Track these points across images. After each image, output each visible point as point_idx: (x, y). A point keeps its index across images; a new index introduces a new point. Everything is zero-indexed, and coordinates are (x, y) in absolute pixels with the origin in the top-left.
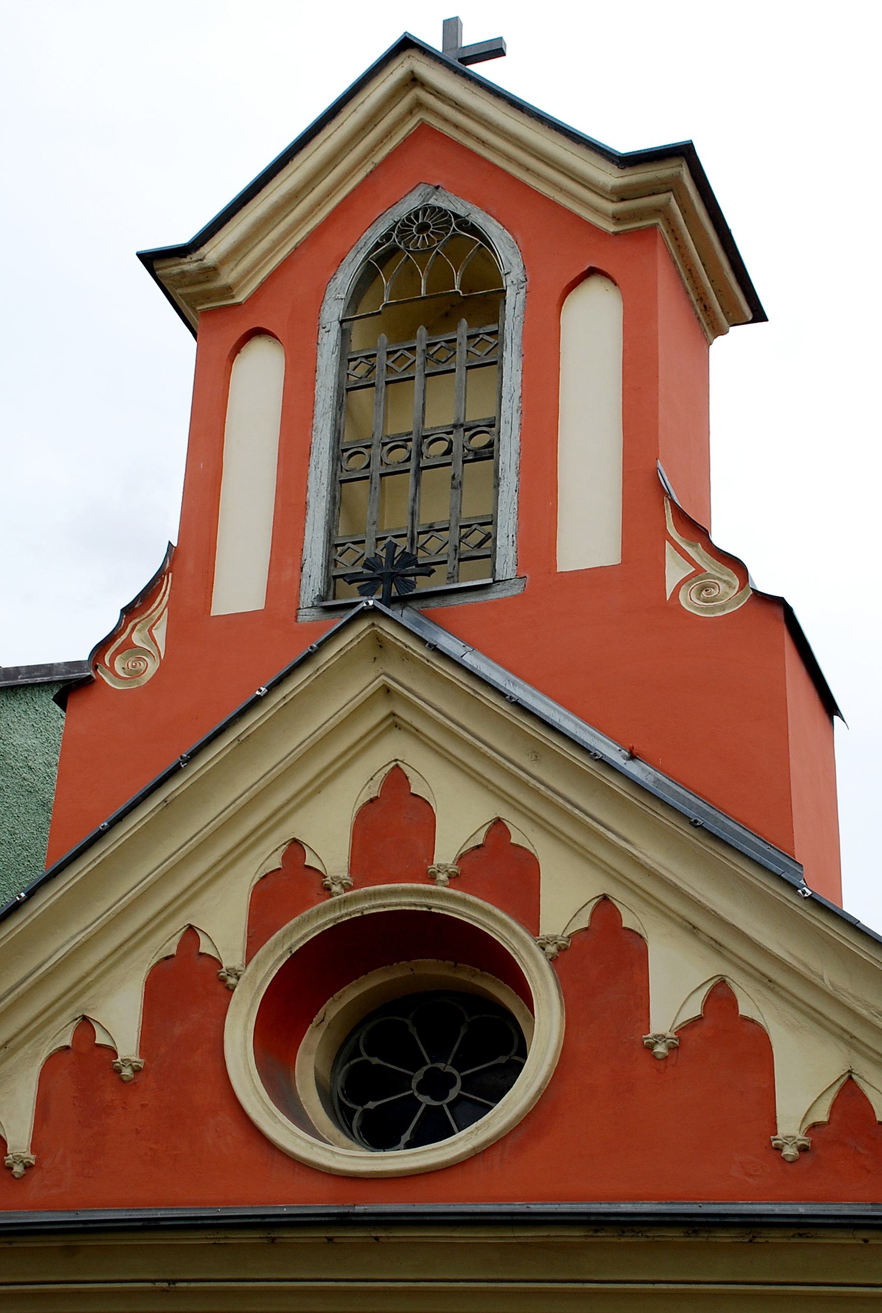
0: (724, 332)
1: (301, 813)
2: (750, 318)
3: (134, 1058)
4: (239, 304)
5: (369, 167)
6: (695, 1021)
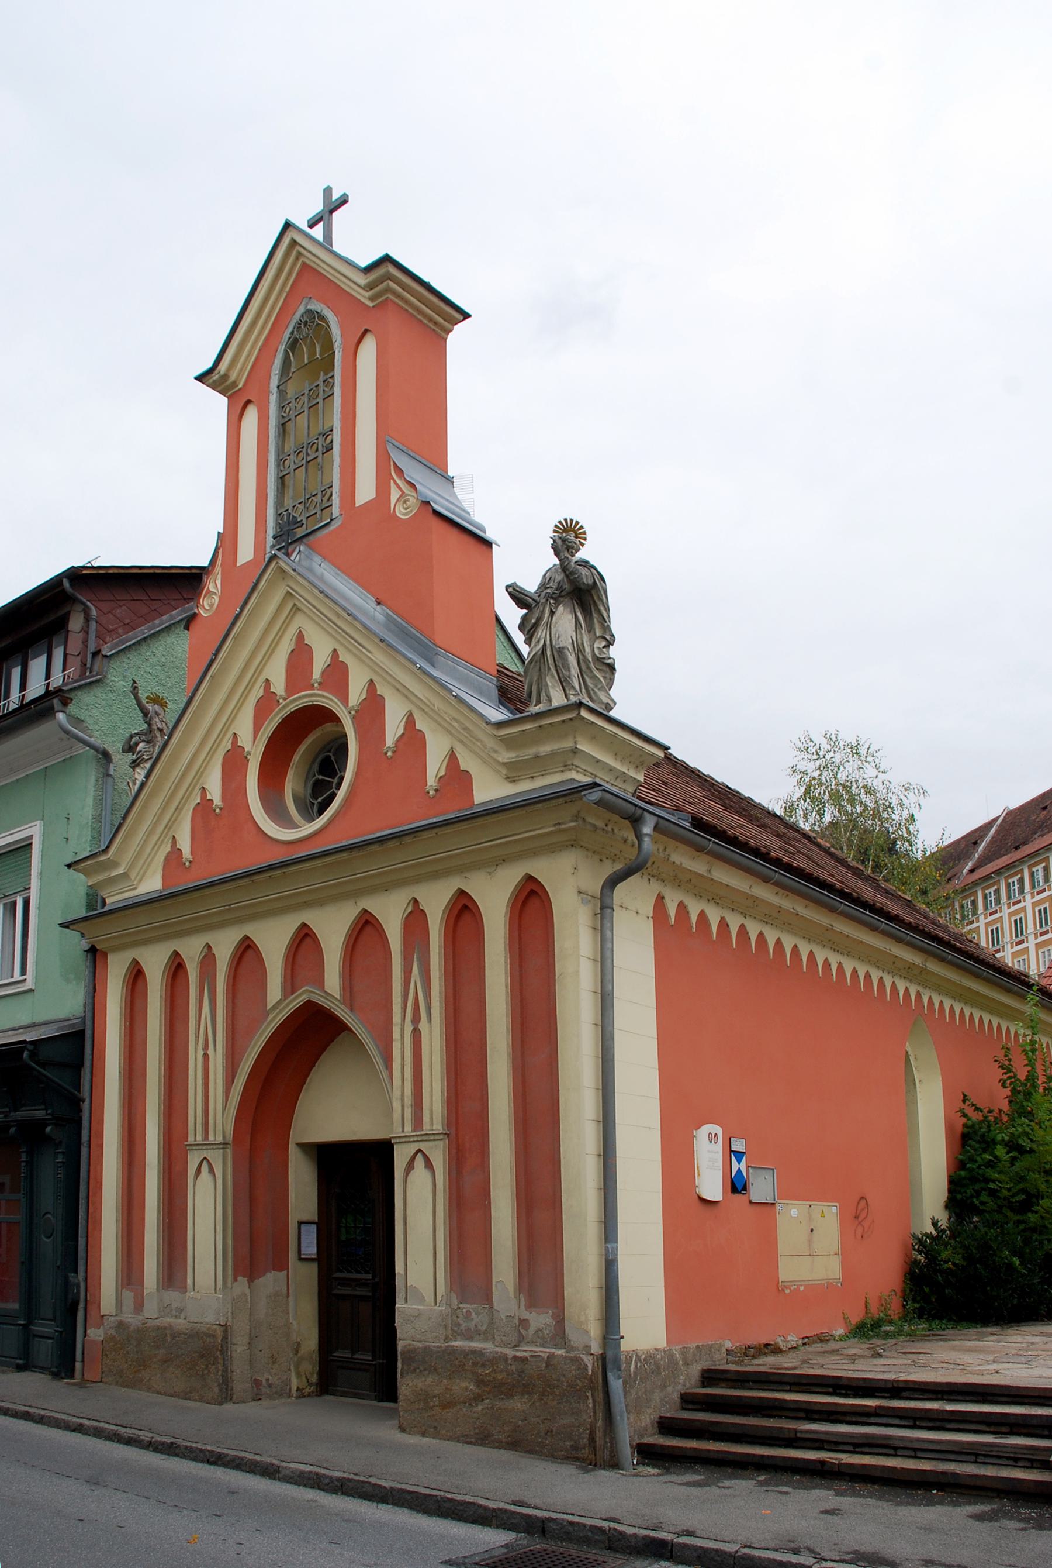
0: (451, 330)
1: (268, 664)
2: (462, 318)
3: (219, 804)
4: (241, 389)
5: (284, 295)
6: (403, 734)
